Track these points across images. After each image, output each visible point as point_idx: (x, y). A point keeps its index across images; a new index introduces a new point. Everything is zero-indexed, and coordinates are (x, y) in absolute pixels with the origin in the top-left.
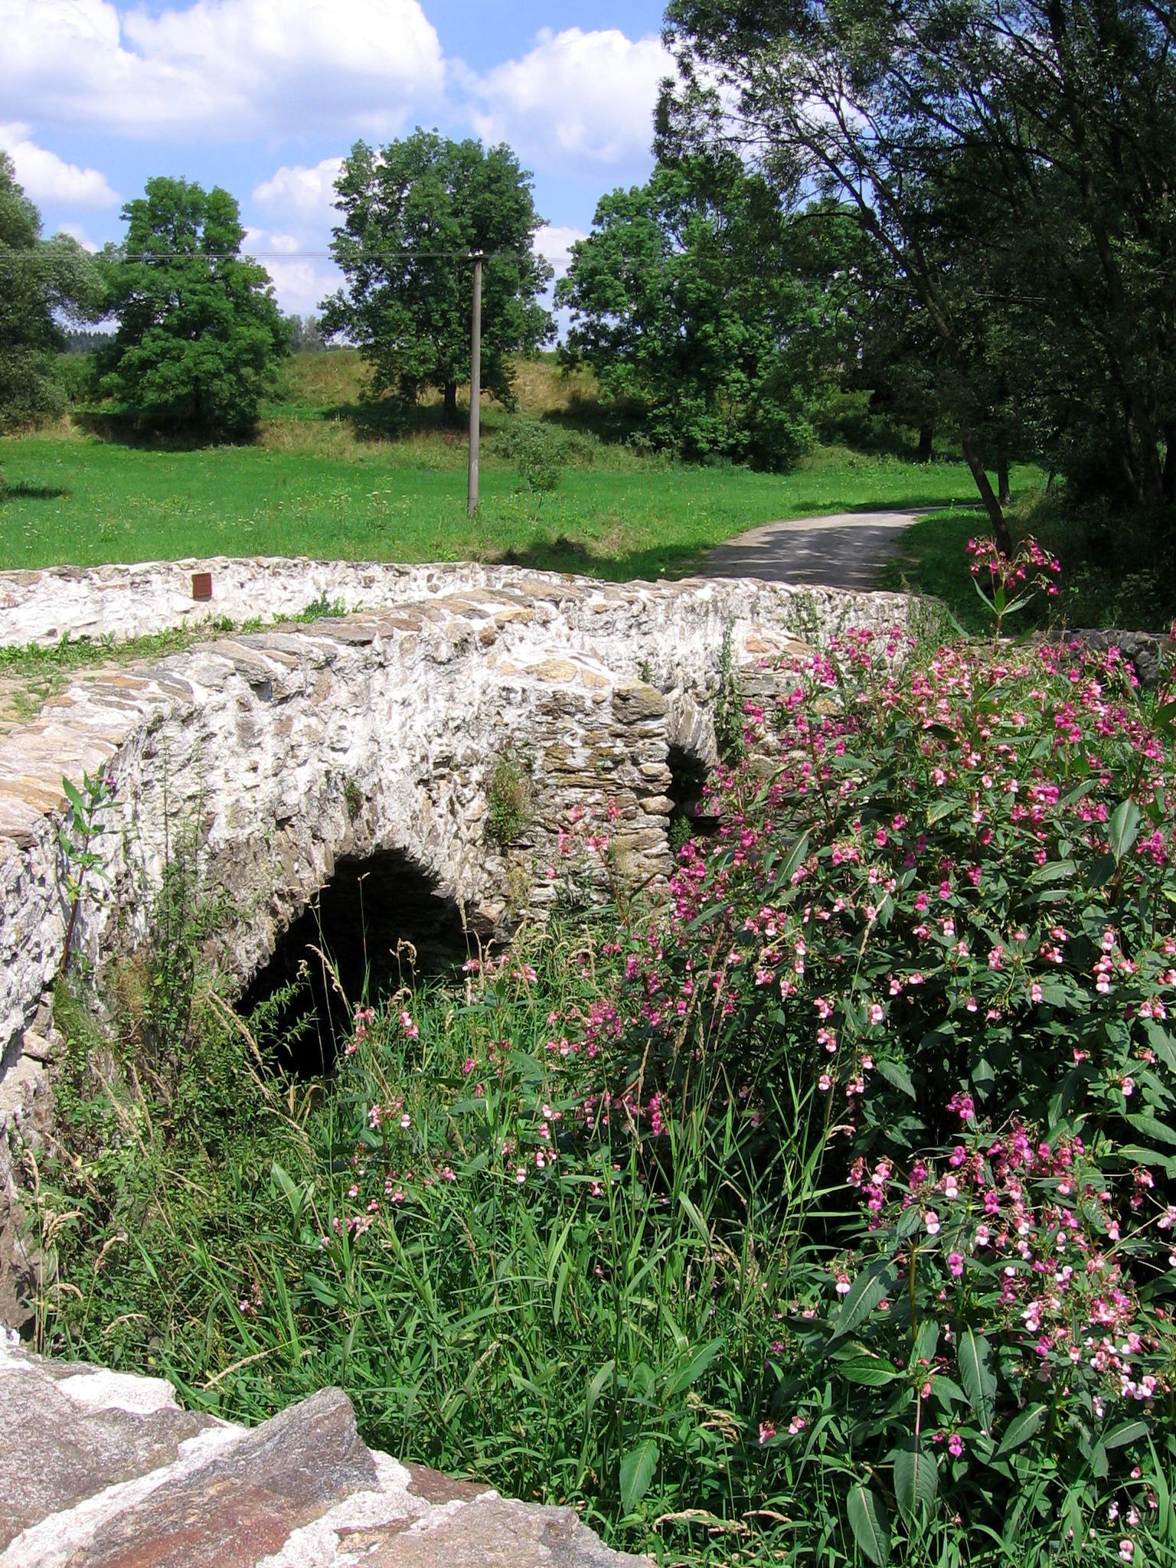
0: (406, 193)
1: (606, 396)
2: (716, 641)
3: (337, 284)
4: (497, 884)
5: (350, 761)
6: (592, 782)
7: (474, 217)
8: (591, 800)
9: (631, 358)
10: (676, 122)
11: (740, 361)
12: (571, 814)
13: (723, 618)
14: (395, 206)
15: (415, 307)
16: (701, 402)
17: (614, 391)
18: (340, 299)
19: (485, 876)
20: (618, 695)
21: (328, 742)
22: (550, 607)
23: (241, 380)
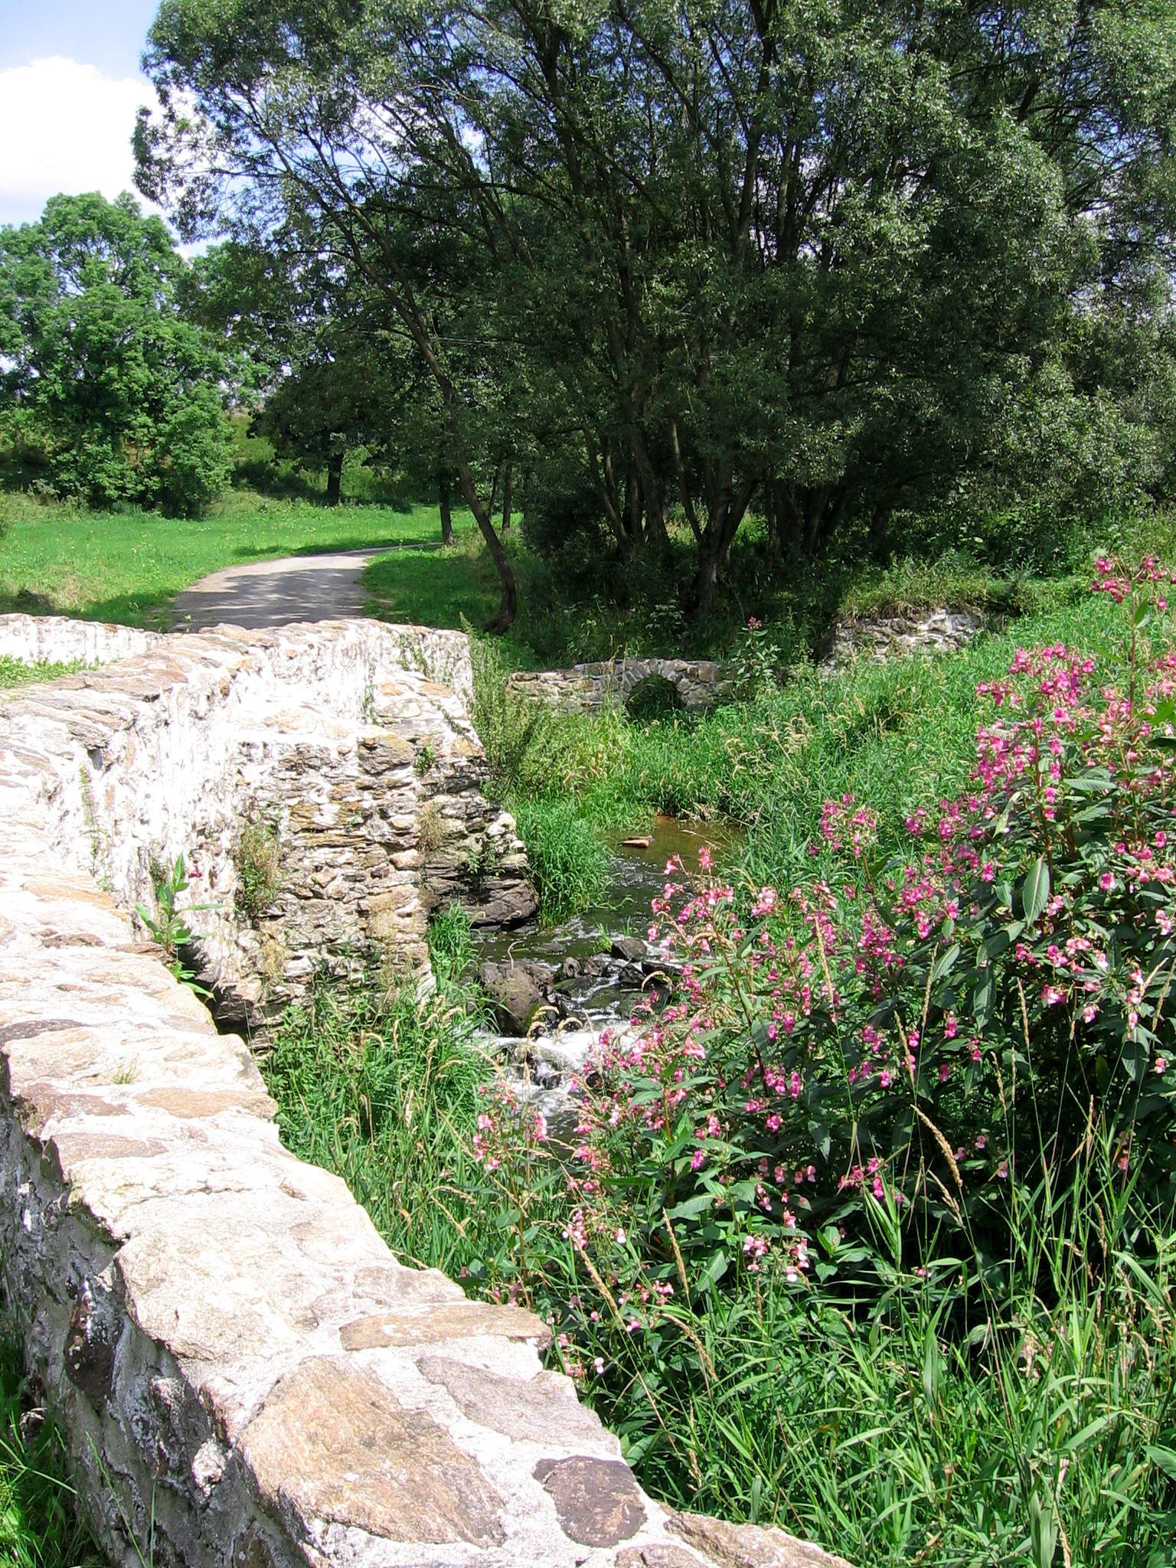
6: (342, 840)
8: (341, 860)
11: (146, 405)
12: (320, 877)
16: (107, 447)
17: (13, 437)
19: (241, 953)
20: (364, 745)
21: (138, 815)
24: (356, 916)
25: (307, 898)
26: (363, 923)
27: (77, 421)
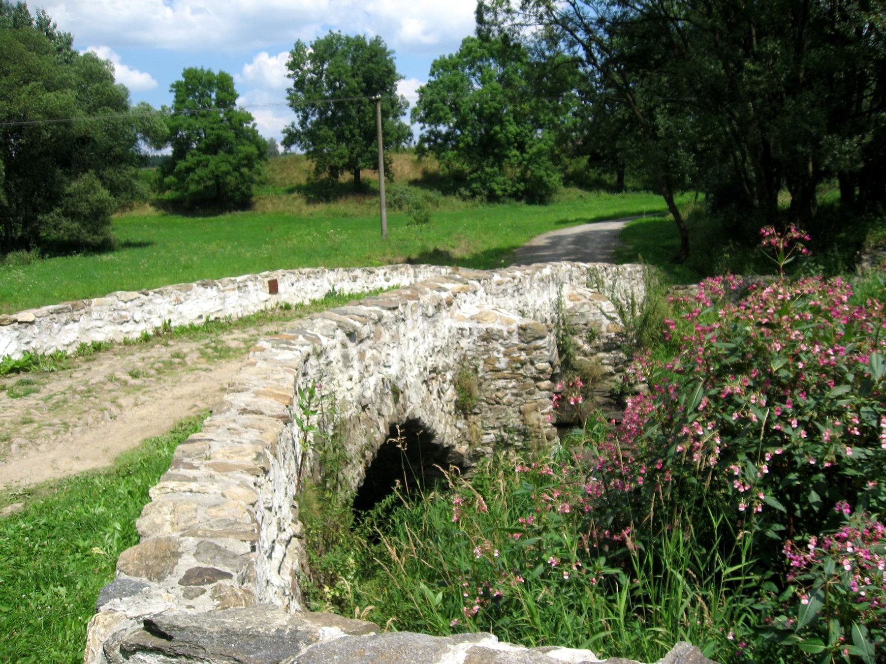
0: (326, 66)
1: (443, 170)
2: (554, 296)
3: (290, 118)
4: (464, 435)
5: (393, 371)
6: (510, 376)
7: (364, 77)
8: (510, 386)
9: (455, 147)
10: (488, 17)
12: (500, 394)
13: (557, 284)
14: (320, 74)
15: (335, 129)
16: (496, 169)
17: (448, 166)
18: (293, 126)
21: (382, 363)
22: (476, 283)
23: (242, 175)
24: (518, 414)
25: (493, 404)
26: (522, 417)
27: (480, 155)
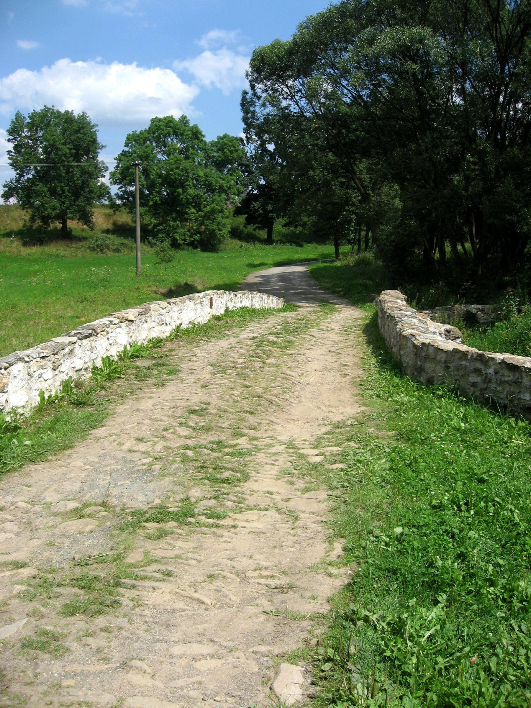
11: (193, 204)
